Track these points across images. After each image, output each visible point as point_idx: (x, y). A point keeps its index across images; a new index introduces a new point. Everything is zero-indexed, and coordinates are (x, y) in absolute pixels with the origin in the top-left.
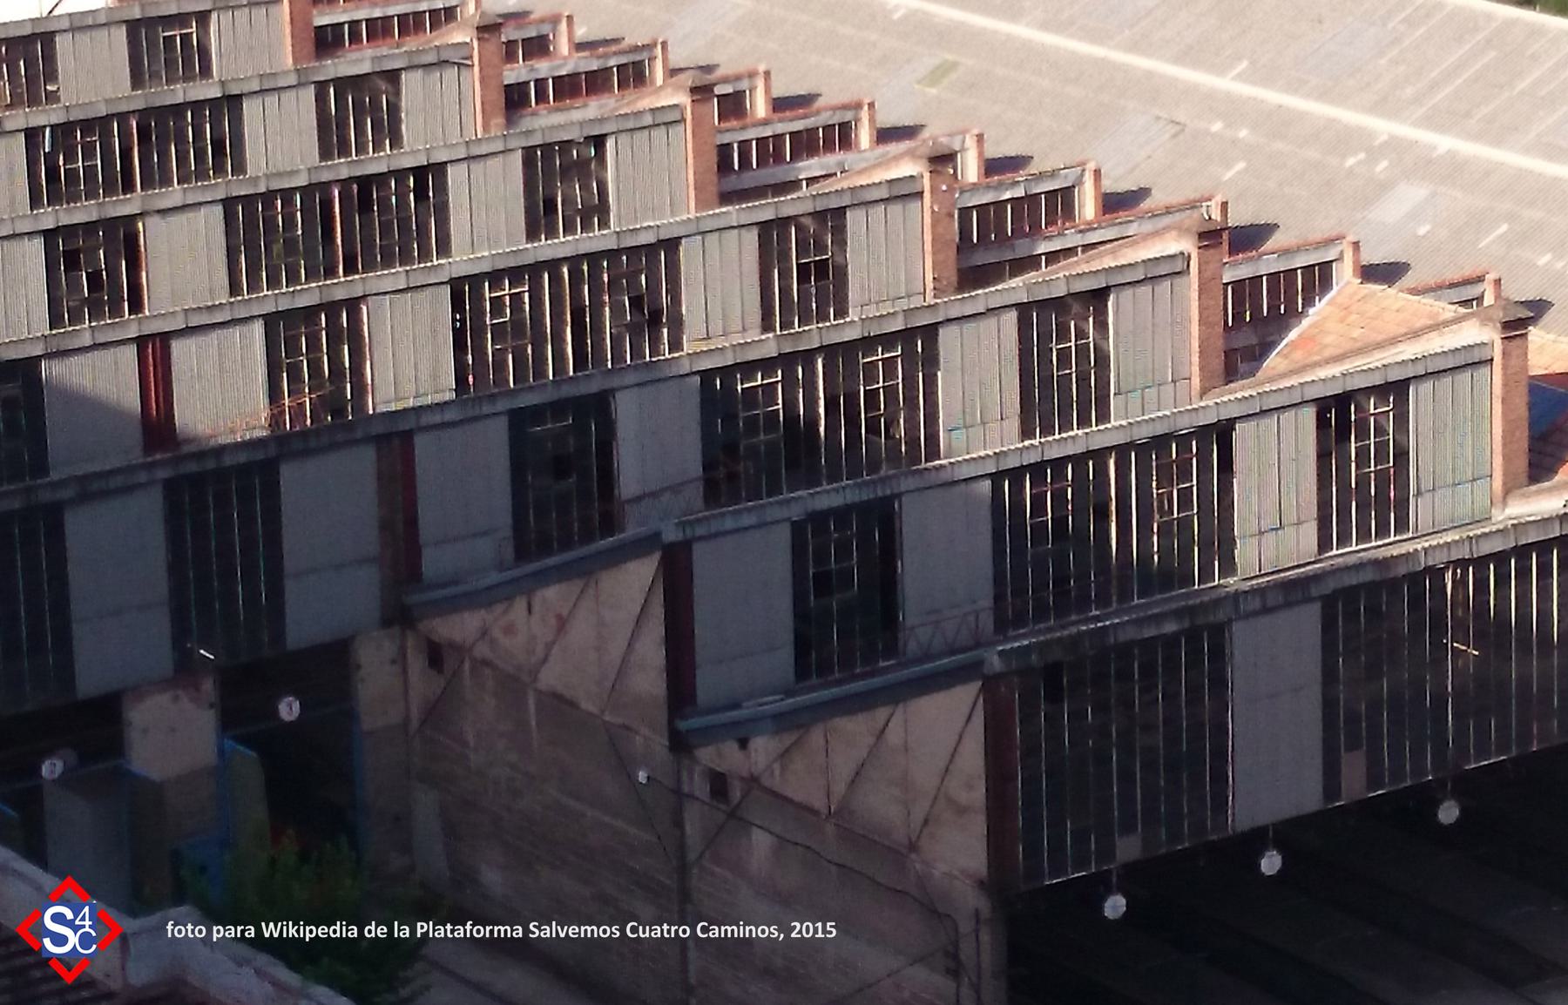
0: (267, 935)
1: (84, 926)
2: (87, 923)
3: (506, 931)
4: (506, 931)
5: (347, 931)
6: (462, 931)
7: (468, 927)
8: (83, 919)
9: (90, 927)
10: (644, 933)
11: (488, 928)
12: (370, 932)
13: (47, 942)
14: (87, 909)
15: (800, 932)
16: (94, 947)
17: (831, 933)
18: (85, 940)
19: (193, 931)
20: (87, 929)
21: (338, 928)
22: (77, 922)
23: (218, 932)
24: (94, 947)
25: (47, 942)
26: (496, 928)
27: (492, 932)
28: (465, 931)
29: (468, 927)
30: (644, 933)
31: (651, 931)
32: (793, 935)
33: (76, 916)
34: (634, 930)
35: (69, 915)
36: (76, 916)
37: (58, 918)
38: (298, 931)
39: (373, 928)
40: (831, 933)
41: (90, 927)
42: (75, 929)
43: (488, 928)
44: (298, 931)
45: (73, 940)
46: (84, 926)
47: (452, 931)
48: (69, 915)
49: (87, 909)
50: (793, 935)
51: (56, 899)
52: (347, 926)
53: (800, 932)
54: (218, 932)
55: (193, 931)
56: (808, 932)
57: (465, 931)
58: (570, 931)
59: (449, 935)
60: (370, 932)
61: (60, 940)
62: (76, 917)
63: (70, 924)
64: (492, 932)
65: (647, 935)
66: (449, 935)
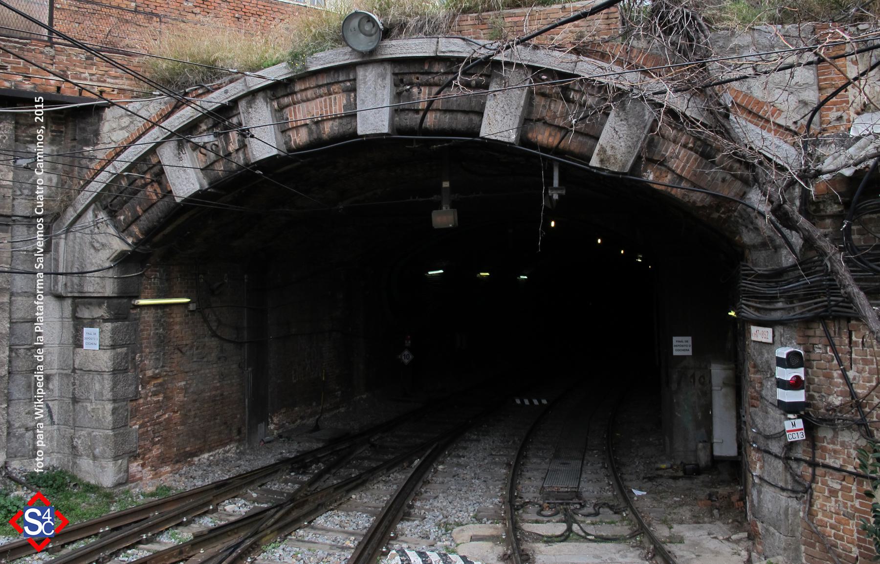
0: (42, 416)
1: (47, 520)
2: (49, 518)
3: (40, 282)
4: (40, 282)
5: (40, 371)
6: (40, 307)
7: (38, 303)
8: (47, 516)
9: (51, 520)
10: (41, 204)
11: (38, 292)
12: (40, 358)
13: (26, 529)
14: (49, 510)
15: (40, 117)
16: (53, 531)
17: (41, 100)
18: (48, 528)
19: (40, 457)
20: (49, 521)
21: (38, 376)
22: (43, 518)
23: (40, 443)
24: (53, 531)
25: (26, 529)
26: (38, 287)
27: (41, 290)
28: (40, 305)
29: (38, 303)
30: (41, 204)
31: (39, 200)
32: (42, 120)
33: (42, 515)
34: (39, 210)
35: (39, 513)
36: (42, 515)
37: (32, 515)
38: (40, 399)
39: (38, 356)
40: (41, 100)
41: (51, 520)
42: (42, 521)
43: (38, 292)
44: (40, 399)
45: (41, 527)
46: (47, 520)
47: (40, 312)
48: (39, 513)
49: (49, 510)
50: (42, 120)
51: (31, 505)
52: (37, 371)
53: (40, 117)
54: (40, 443)
55: (40, 457)
56: (41, 113)
57: (40, 305)
58: (40, 246)
59: (42, 313)
60: (40, 358)
61: (34, 527)
62: (42, 515)
63: (39, 519)
64: (41, 290)
65: (42, 203)
66: (42, 313)
